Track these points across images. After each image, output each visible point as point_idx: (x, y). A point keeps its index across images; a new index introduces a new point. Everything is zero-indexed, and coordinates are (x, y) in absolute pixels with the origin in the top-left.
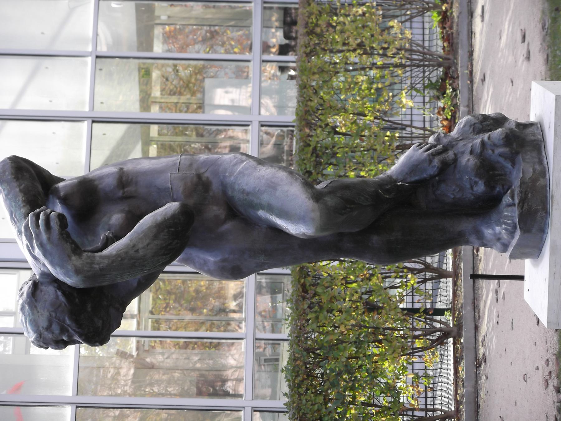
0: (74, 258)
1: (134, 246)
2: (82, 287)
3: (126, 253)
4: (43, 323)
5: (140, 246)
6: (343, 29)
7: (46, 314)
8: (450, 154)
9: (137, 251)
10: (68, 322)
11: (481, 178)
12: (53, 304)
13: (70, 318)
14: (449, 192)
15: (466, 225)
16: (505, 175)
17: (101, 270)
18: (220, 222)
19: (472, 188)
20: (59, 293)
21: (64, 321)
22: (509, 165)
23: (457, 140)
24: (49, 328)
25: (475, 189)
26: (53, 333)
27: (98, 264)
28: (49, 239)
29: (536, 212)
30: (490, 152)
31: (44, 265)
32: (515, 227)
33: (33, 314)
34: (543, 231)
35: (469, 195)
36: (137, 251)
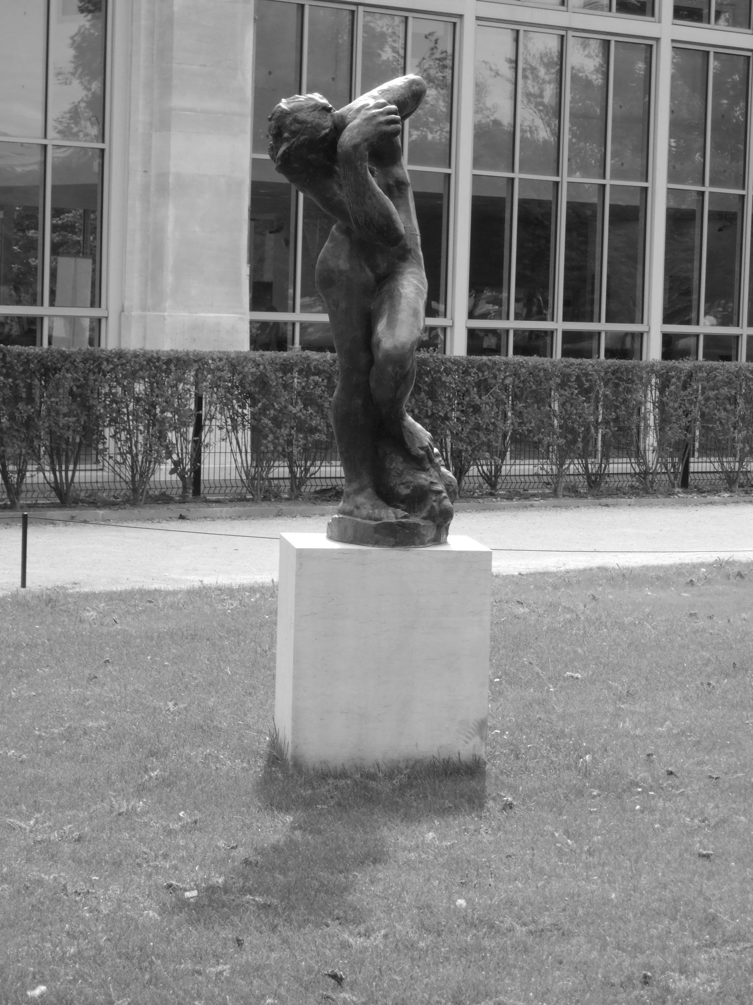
0: (366, 144)
1: (375, 196)
2: (339, 150)
3: (369, 189)
4: (302, 116)
5: (374, 201)
6: (250, 386)
7: (310, 119)
8: (428, 466)
9: (370, 198)
10: (302, 138)
11: (412, 491)
12: (318, 125)
13: (305, 140)
14: (397, 464)
15: (366, 479)
16: (414, 512)
17: (356, 168)
18: (373, 268)
19: (403, 484)
20: (327, 130)
21: (303, 134)
22: (424, 514)
23: (439, 471)
24: (296, 120)
25: (401, 486)
26: (291, 125)
27: (361, 165)
28: (381, 123)
29: (395, 537)
30: (434, 498)
31: (355, 118)
32: (376, 520)
33: (308, 108)
34: (376, 543)
35: (394, 481)
36: (370, 198)
